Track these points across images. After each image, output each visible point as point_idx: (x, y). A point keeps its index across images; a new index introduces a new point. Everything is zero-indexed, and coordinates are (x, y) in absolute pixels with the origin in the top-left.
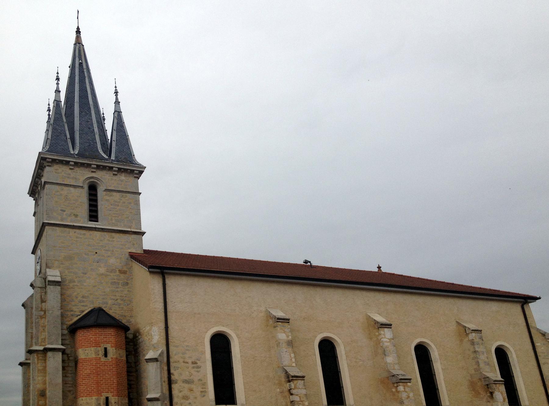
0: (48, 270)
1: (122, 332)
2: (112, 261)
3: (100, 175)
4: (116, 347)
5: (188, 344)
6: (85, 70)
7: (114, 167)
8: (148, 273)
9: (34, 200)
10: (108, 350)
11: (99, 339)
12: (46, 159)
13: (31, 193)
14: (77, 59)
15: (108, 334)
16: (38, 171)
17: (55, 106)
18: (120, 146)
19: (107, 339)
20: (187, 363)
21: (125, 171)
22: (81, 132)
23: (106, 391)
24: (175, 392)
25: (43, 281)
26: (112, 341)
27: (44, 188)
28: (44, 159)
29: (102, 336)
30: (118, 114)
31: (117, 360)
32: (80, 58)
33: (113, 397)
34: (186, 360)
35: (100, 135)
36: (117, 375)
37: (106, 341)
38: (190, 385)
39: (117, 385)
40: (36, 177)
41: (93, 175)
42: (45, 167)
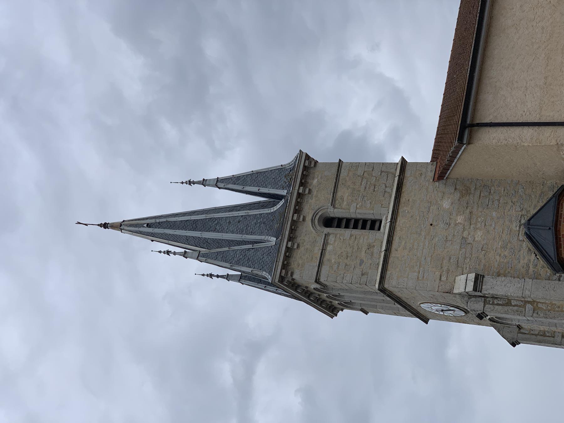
0: (456, 291)
2: (446, 204)
3: (308, 210)
6: (158, 221)
7: (298, 190)
8: (471, 146)
9: (342, 310)
12: (282, 276)
13: (332, 312)
14: (141, 229)
16: (299, 292)
17: (205, 259)
18: (266, 183)
21: (304, 176)
22: (244, 232)
25: (473, 299)
27: (325, 286)
28: (282, 279)
30: (220, 183)
32: (142, 225)
35: (250, 209)
40: (308, 297)
41: (309, 219)
42: (293, 279)
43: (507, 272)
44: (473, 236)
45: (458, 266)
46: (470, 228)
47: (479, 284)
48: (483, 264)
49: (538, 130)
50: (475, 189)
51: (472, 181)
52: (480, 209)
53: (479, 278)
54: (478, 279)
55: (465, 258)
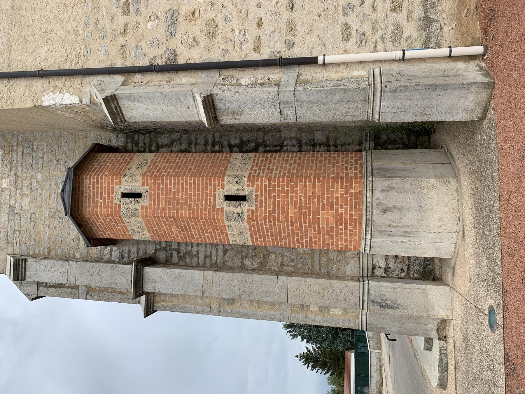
1: (98, 158)
4: (121, 175)
5: (83, 24)
10: (126, 191)
11: (104, 208)
15: (94, 189)
19: (103, 191)
20: (126, 25)
23: (212, 201)
24: (198, 57)
26: (109, 182)
29: (97, 201)
31: (148, 174)
33: (226, 187)
34: (121, 28)
36: (180, 175)
37: (109, 193)
38: (180, 20)
39: (199, 176)
43: (57, 247)
44: (21, 203)
45: (8, 242)
46: (16, 194)
47: (20, 271)
48: (32, 238)
49: (9, 85)
50: (18, 144)
51: (13, 135)
52: (25, 170)
53: (21, 264)
54: (19, 265)
55: (14, 232)
